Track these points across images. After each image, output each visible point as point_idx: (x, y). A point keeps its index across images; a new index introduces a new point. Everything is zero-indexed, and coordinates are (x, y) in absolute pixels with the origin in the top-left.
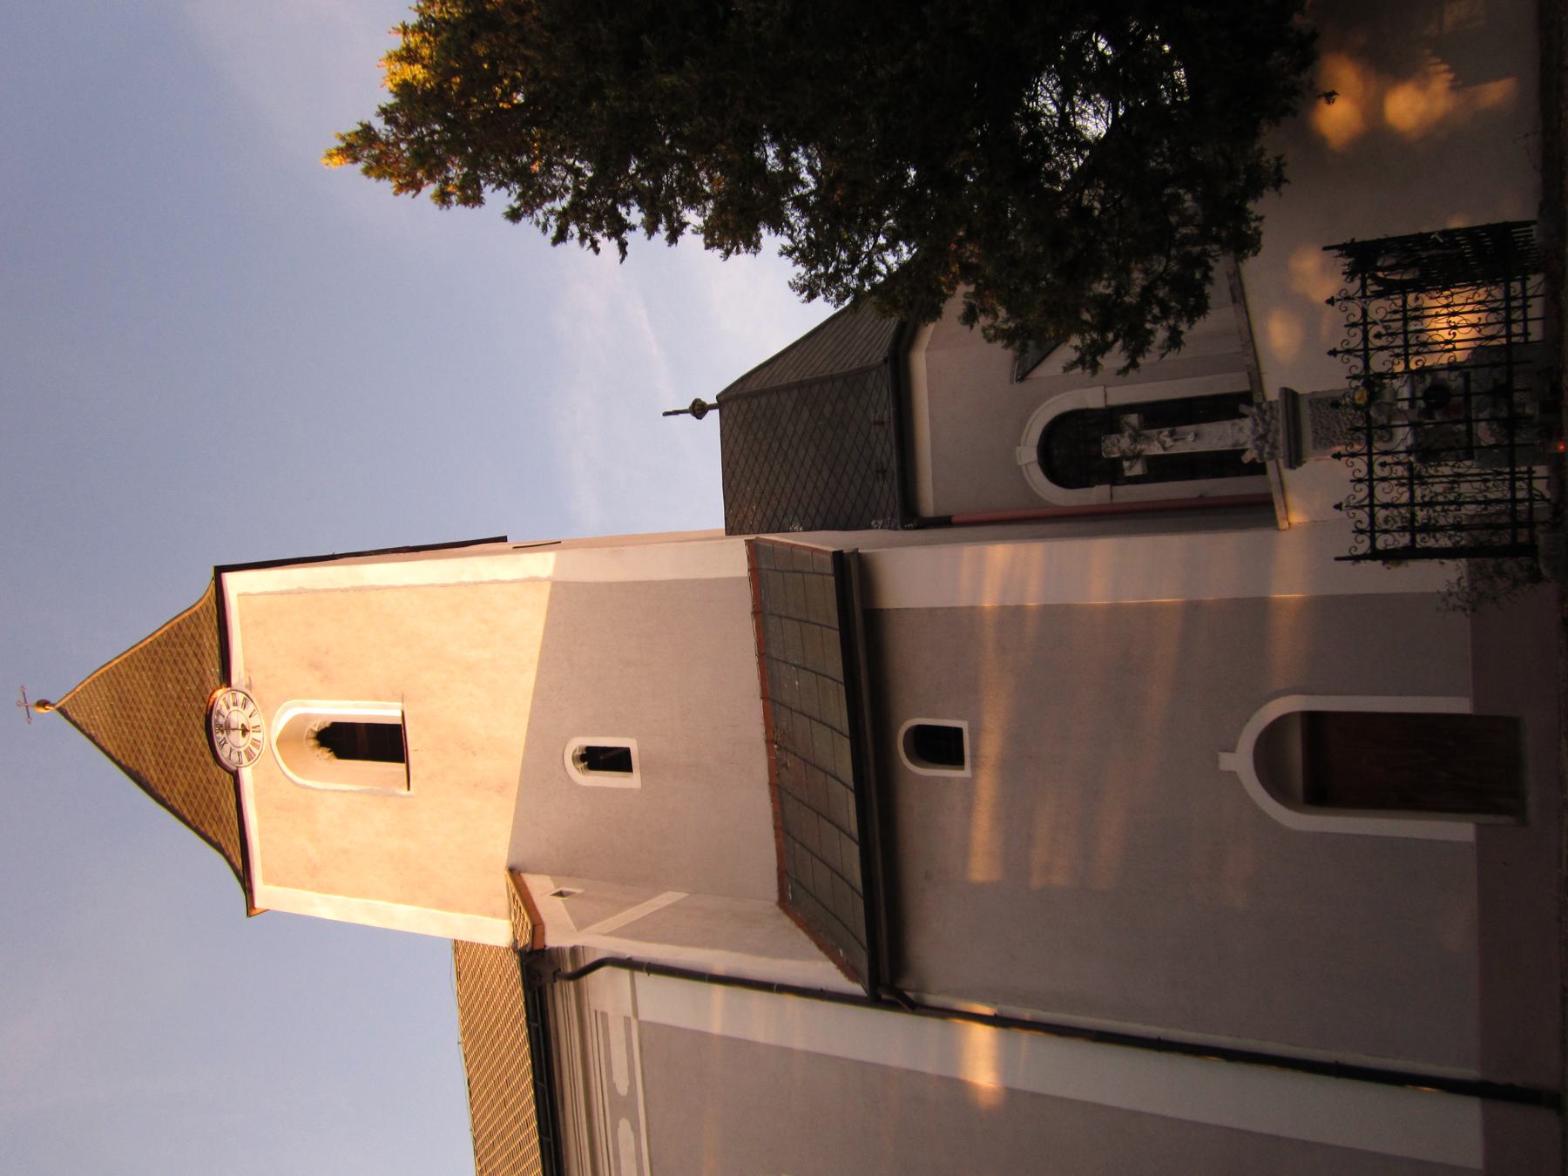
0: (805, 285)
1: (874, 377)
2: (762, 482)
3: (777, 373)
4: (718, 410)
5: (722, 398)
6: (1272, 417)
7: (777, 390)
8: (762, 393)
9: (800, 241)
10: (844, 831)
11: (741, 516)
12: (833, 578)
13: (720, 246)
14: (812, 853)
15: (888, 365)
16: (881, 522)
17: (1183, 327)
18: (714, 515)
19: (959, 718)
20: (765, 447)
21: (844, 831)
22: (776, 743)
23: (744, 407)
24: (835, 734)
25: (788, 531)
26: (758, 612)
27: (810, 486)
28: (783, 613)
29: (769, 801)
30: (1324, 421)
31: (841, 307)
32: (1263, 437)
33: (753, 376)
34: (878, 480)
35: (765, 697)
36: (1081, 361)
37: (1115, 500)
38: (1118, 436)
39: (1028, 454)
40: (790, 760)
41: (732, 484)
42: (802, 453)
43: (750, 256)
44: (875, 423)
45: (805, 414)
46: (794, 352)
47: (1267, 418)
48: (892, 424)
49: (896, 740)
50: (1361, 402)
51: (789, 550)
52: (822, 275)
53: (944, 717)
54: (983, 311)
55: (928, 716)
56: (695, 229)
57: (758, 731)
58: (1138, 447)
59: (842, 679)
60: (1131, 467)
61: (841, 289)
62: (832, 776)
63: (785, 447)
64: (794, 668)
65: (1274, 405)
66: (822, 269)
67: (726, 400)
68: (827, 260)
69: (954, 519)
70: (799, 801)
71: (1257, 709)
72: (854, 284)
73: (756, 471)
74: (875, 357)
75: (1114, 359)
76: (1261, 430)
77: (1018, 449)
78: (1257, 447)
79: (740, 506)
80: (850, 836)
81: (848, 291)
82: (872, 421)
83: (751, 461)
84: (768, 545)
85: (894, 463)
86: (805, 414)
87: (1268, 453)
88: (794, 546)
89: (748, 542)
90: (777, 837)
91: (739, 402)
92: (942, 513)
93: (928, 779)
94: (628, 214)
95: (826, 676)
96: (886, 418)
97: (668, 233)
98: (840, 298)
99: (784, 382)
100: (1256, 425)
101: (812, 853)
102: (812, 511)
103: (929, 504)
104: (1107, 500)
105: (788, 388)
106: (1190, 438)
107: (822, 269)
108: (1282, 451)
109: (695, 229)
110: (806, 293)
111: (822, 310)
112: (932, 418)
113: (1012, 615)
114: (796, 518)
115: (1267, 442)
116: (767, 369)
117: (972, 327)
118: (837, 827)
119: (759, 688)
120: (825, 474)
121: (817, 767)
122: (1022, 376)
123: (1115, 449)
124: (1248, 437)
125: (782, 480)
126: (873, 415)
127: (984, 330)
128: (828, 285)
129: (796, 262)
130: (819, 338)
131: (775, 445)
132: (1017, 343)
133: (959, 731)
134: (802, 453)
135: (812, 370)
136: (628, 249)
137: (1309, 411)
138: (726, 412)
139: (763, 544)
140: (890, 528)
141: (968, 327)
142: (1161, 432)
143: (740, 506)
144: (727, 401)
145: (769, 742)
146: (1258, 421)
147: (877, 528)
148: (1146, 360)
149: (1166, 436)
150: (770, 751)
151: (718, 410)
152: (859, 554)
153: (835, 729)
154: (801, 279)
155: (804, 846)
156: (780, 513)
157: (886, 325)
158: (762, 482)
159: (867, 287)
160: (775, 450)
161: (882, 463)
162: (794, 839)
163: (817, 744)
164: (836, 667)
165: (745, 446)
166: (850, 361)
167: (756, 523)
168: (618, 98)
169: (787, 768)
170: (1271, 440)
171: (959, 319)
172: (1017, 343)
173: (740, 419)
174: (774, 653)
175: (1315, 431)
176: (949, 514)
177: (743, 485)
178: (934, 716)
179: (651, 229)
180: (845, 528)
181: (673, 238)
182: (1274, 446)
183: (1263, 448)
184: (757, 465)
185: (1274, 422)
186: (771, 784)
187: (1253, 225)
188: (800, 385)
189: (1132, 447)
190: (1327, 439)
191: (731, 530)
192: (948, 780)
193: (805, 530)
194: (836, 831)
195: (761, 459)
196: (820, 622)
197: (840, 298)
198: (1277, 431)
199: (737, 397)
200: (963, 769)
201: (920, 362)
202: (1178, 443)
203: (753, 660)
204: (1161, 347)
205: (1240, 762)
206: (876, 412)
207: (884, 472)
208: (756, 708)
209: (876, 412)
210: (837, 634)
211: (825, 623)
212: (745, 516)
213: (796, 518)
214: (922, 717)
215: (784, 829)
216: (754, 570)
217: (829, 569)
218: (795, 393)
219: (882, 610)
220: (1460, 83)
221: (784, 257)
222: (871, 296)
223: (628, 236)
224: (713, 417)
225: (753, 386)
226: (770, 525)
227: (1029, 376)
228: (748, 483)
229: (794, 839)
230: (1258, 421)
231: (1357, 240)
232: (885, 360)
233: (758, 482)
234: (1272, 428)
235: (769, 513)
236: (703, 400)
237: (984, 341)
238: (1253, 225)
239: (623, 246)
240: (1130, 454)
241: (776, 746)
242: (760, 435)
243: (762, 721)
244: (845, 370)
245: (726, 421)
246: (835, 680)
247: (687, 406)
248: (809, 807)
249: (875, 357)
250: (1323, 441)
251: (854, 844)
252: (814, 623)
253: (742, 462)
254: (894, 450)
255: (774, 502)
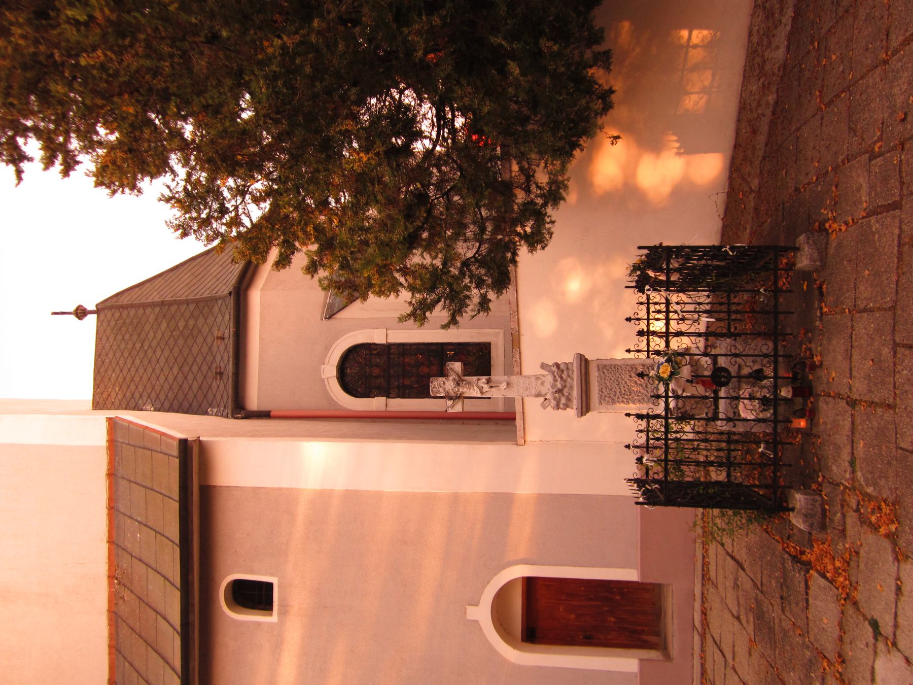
0: (179, 225)
1: (219, 305)
2: (125, 371)
3: (145, 293)
4: (96, 315)
5: (100, 306)
6: (569, 376)
7: (144, 306)
8: (132, 306)
9: (177, 192)
10: (168, 663)
11: (106, 394)
12: (177, 460)
13: (108, 187)
14: (139, 674)
15: (232, 297)
16: (215, 410)
17: (491, 295)
18: (85, 389)
19: (272, 575)
20: (130, 346)
21: (168, 663)
22: (117, 579)
23: (117, 315)
24: (167, 583)
25: (142, 410)
26: (112, 475)
27: (162, 378)
28: (132, 479)
29: (107, 625)
30: (608, 382)
31: (210, 247)
32: (560, 391)
33: (126, 294)
34: (216, 379)
35: (111, 541)
36: (413, 314)
37: (389, 409)
38: (444, 379)
39: (330, 371)
40: (127, 595)
41: (101, 370)
42: (158, 353)
43: (133, 197)
44: (218, 338)
45: (164, 325)
46: (160, 279)
47: (564, 376)
48: (231, 340)
49: (218, 591)
50: (665, 376)
51: (142, 430)
52: (195, 219)
53: (259, 574)
54: (323, 266)
55: (246, 572)
56: (88, 172)
57: (101, 568)
58: (461, 390)
59: (178, 542)
60: (453, 406)
61: (210, 233)
62: (162, 616)
63: (146, 348)
64: (137, 523)
65: (570, 366)
66: (194, 215)
67: (102, 309)
68: (200, 208)
69: (272, 414)
70: (132, 629)
71: (495, 574)
72: (223, 229)
73: (121, 362)
74: (221, 290)
75: (440, 313)
76: (559, 386)
77: (323, 366)
78: (555, 398)
79: (106, 387)
80: (173, 669)
81: (217, 234)
82: (216, 335)
83: (118, 354)
84: (125, 424)
85: (230, 369)
86: (164, 325)
87: (564, 404)
88: (147, 428)
89: (109, 420)
90: (110, 654)
91: (113, 310)
92: (264, 408)
93: (243, 623)
94: (25, 144)
95: (163, 535)
96: (226, 335)
97: (62, 167)
98: (210, 239)
99: (150, 300)
100: (555, 380)
101: (139, 674)
102: (162, 397)
103: (254, 401)
104: (383, 408)
105: (153, 305)
106: (504, 386)
107: (194, 215)
108: (575, 403)
109: (88, 172)
110: (180, 232)
111: (194, 246)
112: (261, 339)
113: (323, 497)
114: (149, 400)
115: (563, 395)
116: (137, 289)
117: (313, 276)
118: (163, 658)
119: (107, 534)
120: (176, 370)
121: (149, 606)
122: (330, 314)
123: (441, 390)
124: (549, 389)
125: (141, 371)
126: (216, 332)
127: (320, 281)
128: (200, 227)
129: (173, 206)
130: (179, 273)
131: (138, 345)
132: (346, 293)
133: (270, 586)
134: (158, 353)
135: (173, 294)
136: (23, 176)
137: (597, 374)
138: (102, 317)
139: (120, 422)
140: (222, 416)
141: (309, 276)
142: (479, 380)
143: (106, 387)
144: (103, 309)
145: (111, 577)
146: (557, 377)
147: (212, 415)
148: (463, 319)
149: (483, 383)
150: (111, 585)
151: (96, 315)
152: (200, 441)
153: (168, 580)
154: (176, 220)
155: (132, 666)
156: (137, 395)
157: (232, 269)
158: (125, 371)
159: (234, 234)
160: (138, 349)
161: (220, 367)
162: (125, 658)
163: (150, 587)
164: (174, 531)
165: (115, 343)
166: (202, 291)
167: (117, 400)
168: (23, 37)
169: (124, 600)
170: (566, 394)
171: (302, 269)
172: (346, 293)
173: (113, 323)
174: (122, 508)
175: (601, 390)
176: (269, 409)
177: (110, 372)
178: (252, 572)
179: (49, 162)
180: (187, 411)
181: (66, 172)
182: (569, 399)
183: (560, 399)
184: (122, 358)
185: (569, 380)
186: (110, 611)
187: (547, 226)
188: (163, 304)
189: (456, 389)
190: (609, 397)
191: (98, 404)
192: (259, 624)
193: (155, 410)
194: (162, 661)
195: (126, 355)
196: (163, 492)
197: (210, 239)
198: (571, 387)
199: (111, 308)
200: (271, 615)
201: (256, 297)
202: (493, 390)
203: (104, 512)
204: (473, 310)
205: (482, 613)
206: (219, 330)
207: (221, 374)
208: (101, 550)
209: (219, 330)
210: (177, 505)
211: (167, 494)
212: (109, 395)
213: (149, 400)
214: (233, 573)
215: (115, 648)
216: (112, 443)
217: (175, 452)
218: (157, 310)
219: (215, 487)
220: (682, 151)
221: (162, 202)
222: (235, 240)
223: (25, 165)
224: (92, 319)
225: (125, 300)
226: (128, 404)
227: (335, 316)
228: (114, 371)
229: (125, 658)
230: (557, 377)
231: (663, 245)
232: (230, 294)
233: (121, 371)
234: (568, 385)
235: (128, 395)
236: (85, 306)
237: (320, 288)
238: (547, 226)
239: (19, 173)
240: (454, 395)
241: (116, 581)
242: (127, 336)
243: (107, 560)
244: (198, 297)
245: (102, 324)
246: (172, 541)
247: (72, 309)
248: (139, 636)
249: (221, 290)
250: (607, 399)
251: (176, 677)
252: (157, 492)
253: (111, 355)
254: (231, 359)
255: (133, 387)
